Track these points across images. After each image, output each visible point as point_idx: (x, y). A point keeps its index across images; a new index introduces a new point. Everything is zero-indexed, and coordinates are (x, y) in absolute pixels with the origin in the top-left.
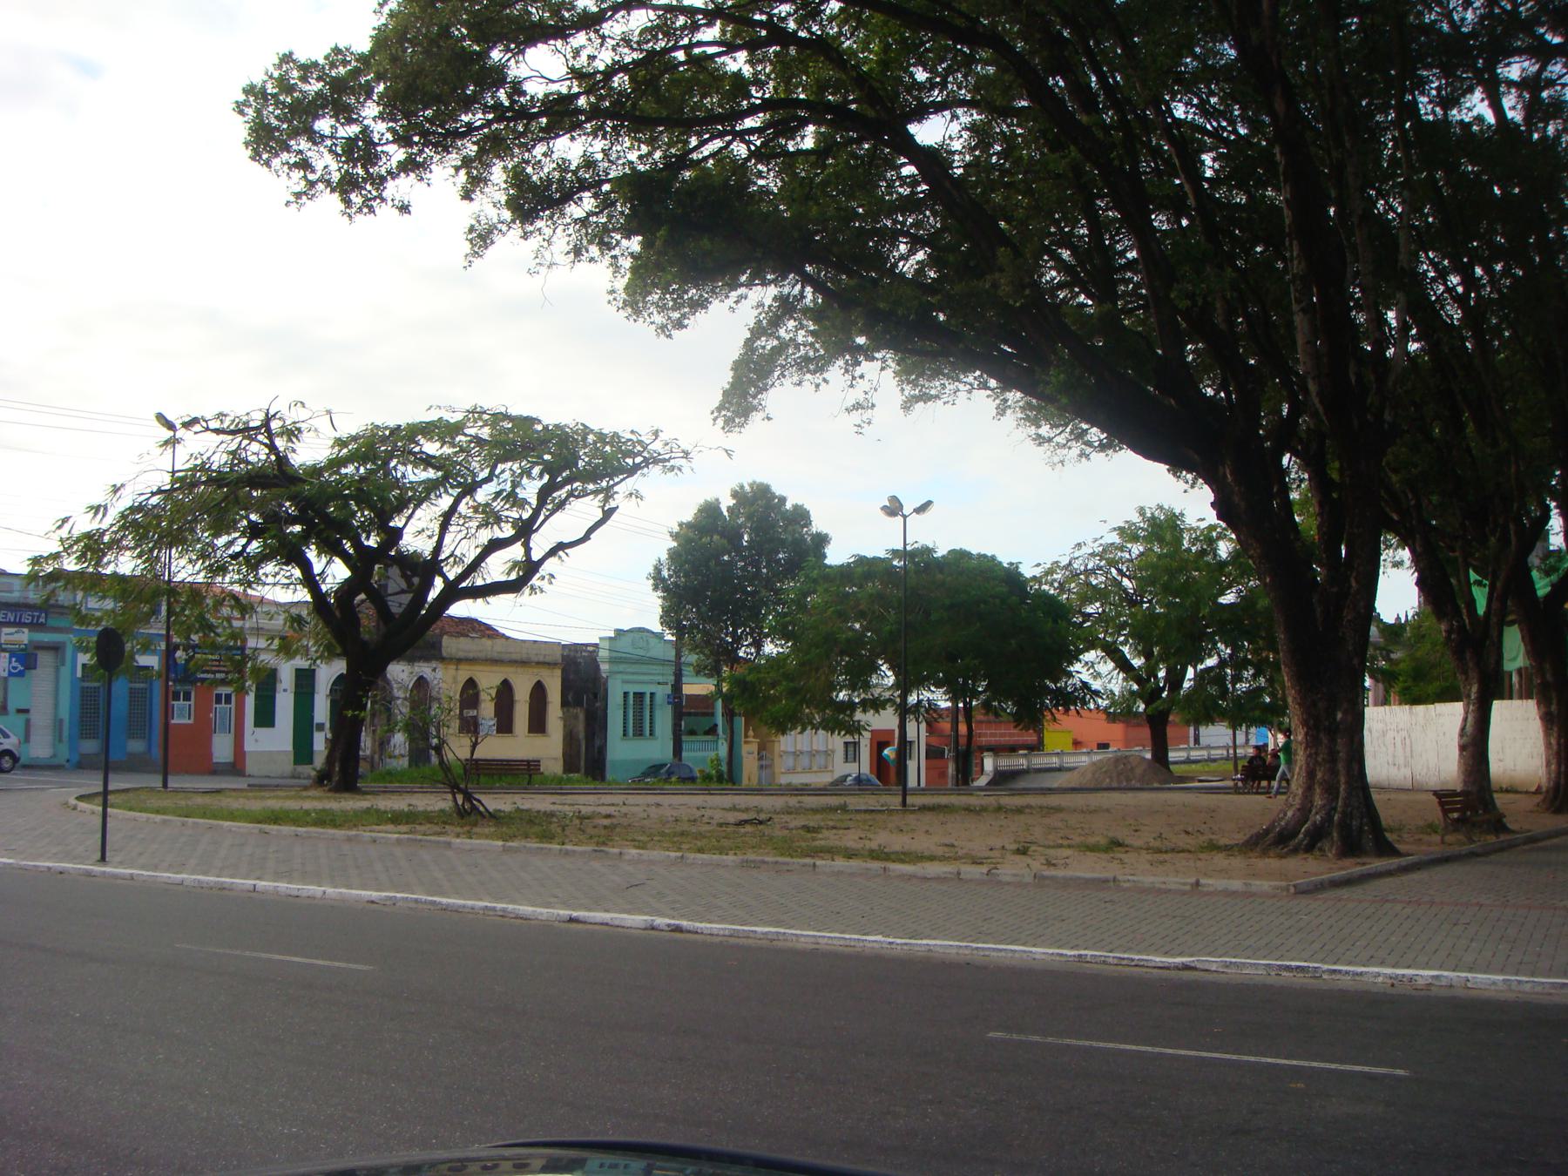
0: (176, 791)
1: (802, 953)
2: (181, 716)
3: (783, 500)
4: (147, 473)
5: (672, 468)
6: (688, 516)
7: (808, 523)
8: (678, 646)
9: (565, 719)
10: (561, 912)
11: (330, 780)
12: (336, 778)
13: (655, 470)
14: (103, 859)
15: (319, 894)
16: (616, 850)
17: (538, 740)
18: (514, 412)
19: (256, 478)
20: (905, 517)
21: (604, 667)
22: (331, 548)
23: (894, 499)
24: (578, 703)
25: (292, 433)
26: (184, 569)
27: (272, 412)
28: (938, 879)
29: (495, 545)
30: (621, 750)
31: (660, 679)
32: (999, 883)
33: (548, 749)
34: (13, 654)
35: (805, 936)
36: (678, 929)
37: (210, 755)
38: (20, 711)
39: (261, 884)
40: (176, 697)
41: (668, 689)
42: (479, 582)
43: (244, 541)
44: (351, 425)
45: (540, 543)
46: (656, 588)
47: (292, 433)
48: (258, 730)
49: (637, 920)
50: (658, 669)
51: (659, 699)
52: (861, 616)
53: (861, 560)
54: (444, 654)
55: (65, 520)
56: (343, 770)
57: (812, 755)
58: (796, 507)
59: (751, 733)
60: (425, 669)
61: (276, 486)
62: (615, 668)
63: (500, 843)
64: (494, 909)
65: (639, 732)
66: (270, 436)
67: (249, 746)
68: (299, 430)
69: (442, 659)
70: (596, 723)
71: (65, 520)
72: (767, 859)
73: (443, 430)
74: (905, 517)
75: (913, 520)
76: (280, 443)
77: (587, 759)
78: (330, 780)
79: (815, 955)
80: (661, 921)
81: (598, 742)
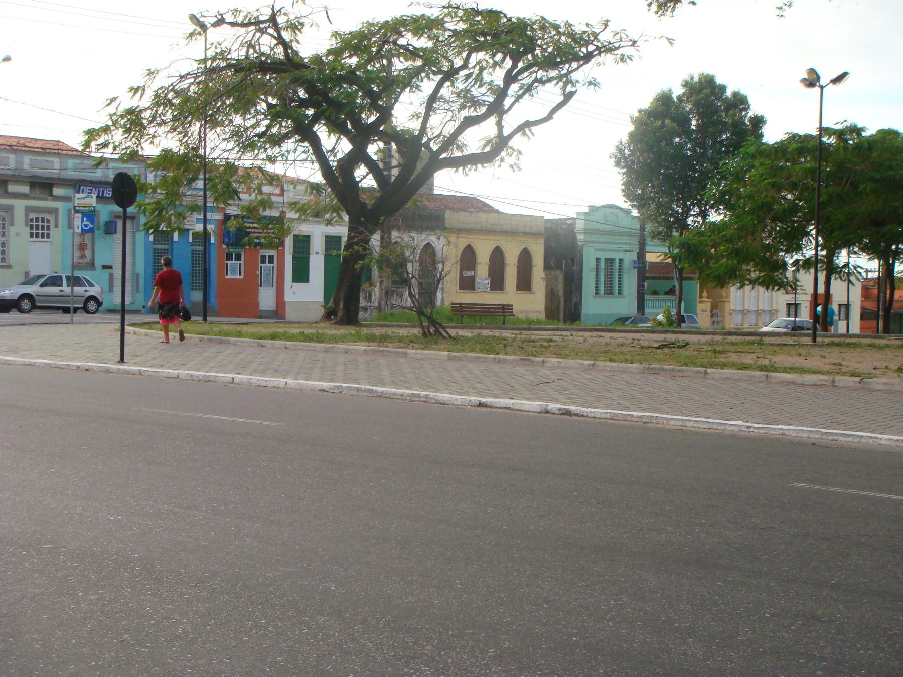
0: (212, 323)
1: (673, 432)
2: (234, 273)
3: (723, 88)
4: (178, 60)
5: (622, 59)
6: (646, 102)
7: (747, 109)
8: (643, 221)
9: (547, 279)
10: (473, 398)
11: (336, 315)
12: (340, 314)
13: (608, 58)
14: (122, 360)
15: (282, 385)
16: (540, 359)
17: (525, 296)
18: (481, 7)
19: (264, 66)
20: (822, 87)
21: (580, 237)
22: (337, 128)
23: (812, 71)
24: (558, 267)
25: (295, 27)
26: (218, 146)
27: (277, 8)
28: (814, 385)
29: (469, 122)
30: (593, 305)
31: (628, 247)
32: (871, 390)
33: (531, 304)
34: (84, 214)
35: (674, 419)
36: (568, 413)
37: (257, 304)
38: (104, 267)
39: (238, 377)
40: (229, 257)
41: (634, 256)
42: (458, 154)
43: (267, 122)
44: (351, 24)
45: (511, 122)
46: (617, 164)
47: (295, 27)
48: (296, 285)
49: (534, 405)
50: (625, 239)
51: (627, 264)
52: (793, 187)
53: (794, 137)
54: (447, 225)
55: (113, 100)
56: (347, 308)
57: (752, 305)
58: (736, 95)
59: (705, 294)
60: (433, 239)
61: (285, 71)
62: (589, 238)
63: (446, 353)
64: (419, 395)
65: (609, 292)
66: (278, 29)
67: (288, 297)
68: (302, 24)
69: (444, 229)
70: (573, 283)
71: (113, 100)
72: (665, 367)
73: (421, 25)
74: (822, 87)
75: (830, 90)
76: (286, 35)
77: (565, 309)
78: (336, 315)
79: (683, 432)
80: (553, 406)
81: (574, 300)
